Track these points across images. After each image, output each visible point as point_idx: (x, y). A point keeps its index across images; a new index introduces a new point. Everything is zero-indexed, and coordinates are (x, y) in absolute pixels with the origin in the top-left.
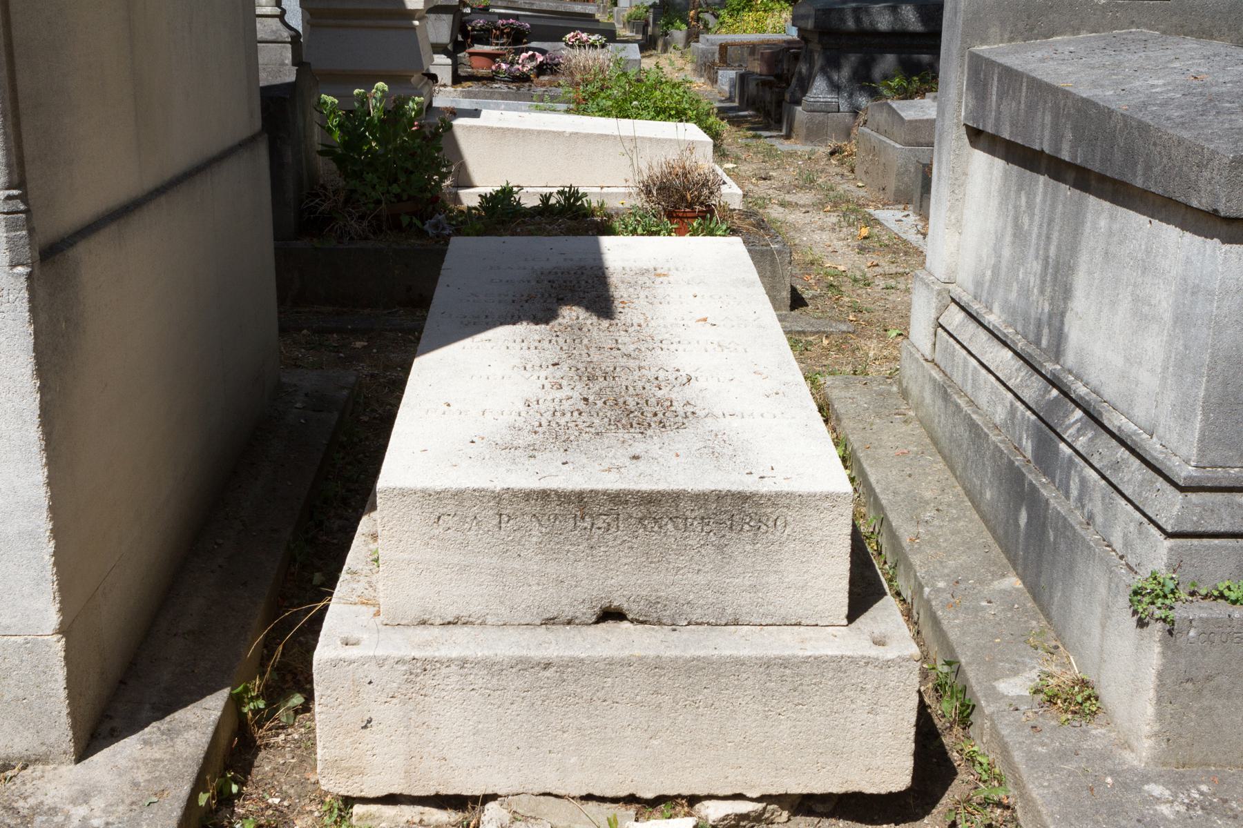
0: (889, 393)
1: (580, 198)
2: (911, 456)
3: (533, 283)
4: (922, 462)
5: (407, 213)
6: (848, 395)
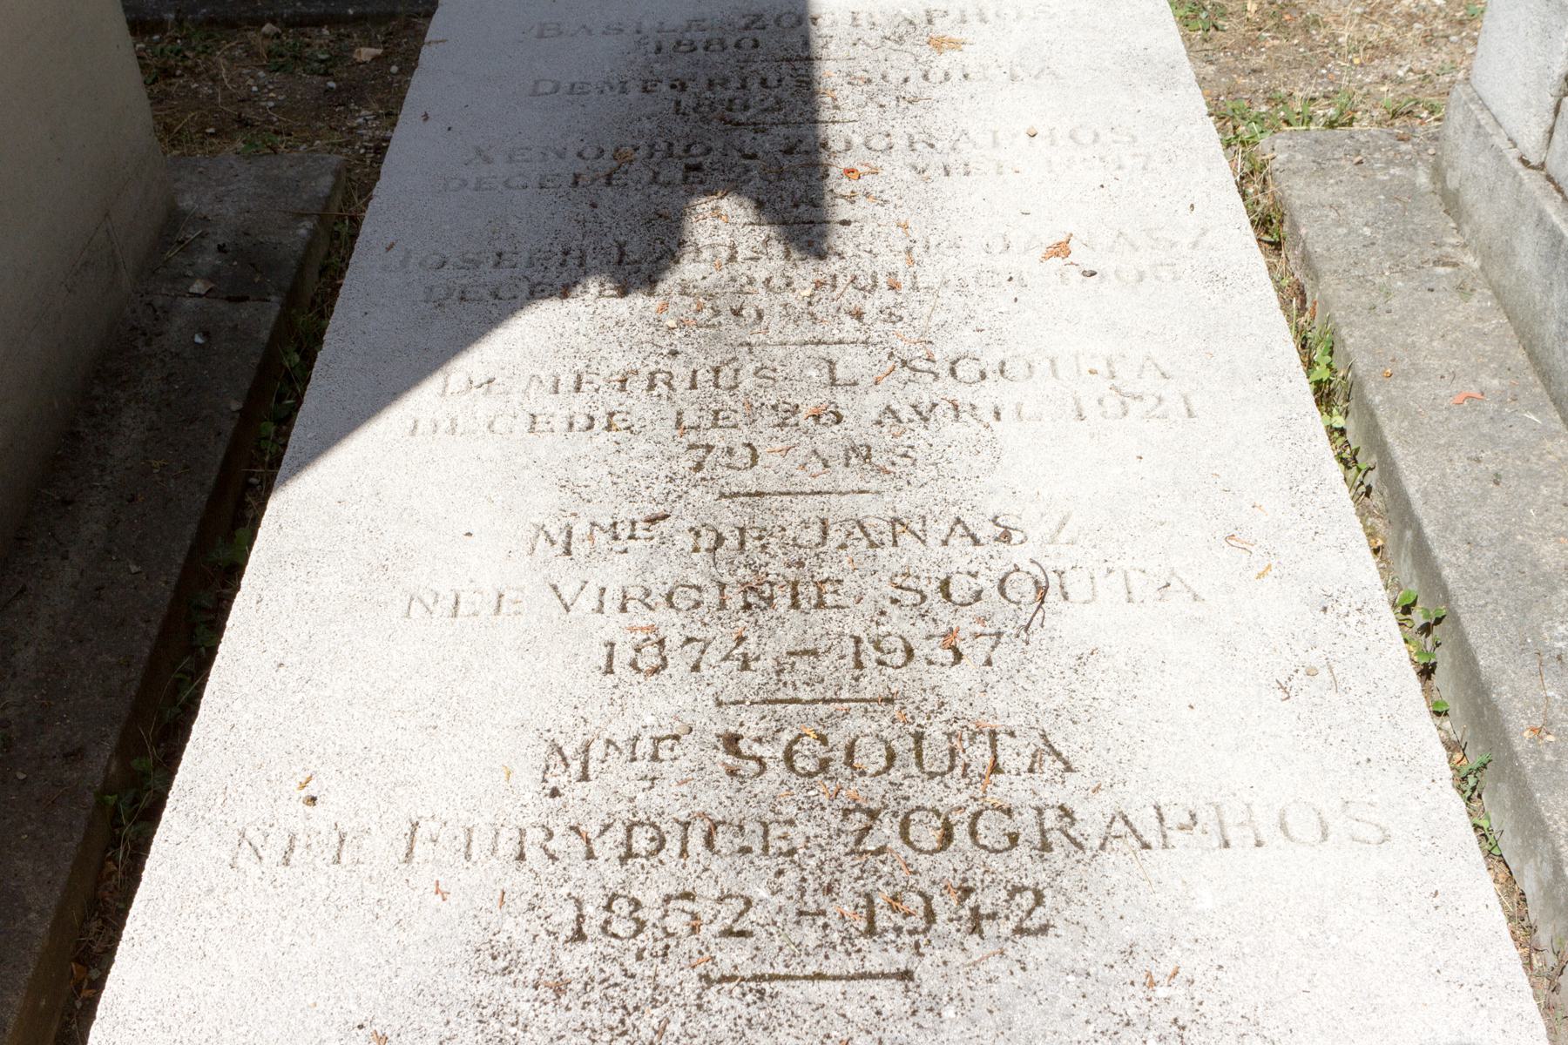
0: (1413, 189)
2: (1491, 406)
3: (634, 93)
4: (1519, 433)
6: (1326, 196)
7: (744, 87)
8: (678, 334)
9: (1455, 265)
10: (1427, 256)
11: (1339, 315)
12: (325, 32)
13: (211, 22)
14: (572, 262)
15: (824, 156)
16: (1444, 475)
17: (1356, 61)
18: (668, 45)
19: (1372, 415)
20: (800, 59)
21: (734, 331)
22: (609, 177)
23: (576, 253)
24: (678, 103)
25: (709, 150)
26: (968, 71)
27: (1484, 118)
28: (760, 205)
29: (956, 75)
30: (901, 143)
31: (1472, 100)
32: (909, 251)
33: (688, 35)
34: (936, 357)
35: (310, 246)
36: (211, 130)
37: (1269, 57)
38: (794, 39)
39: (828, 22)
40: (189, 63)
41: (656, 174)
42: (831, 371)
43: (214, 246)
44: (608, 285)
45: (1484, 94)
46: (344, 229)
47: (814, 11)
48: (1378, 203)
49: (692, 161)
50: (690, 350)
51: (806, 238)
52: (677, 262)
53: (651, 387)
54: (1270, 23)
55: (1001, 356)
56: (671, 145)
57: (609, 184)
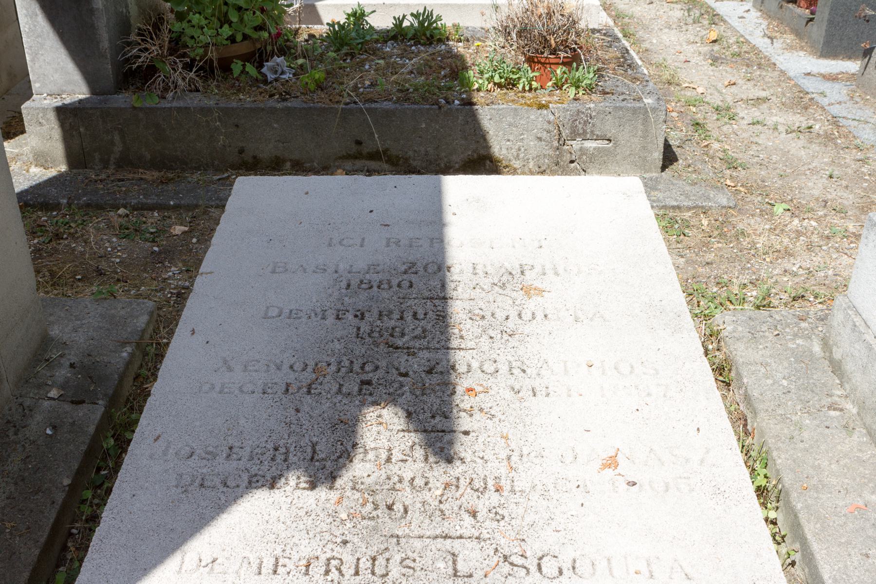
1: (435, 22)
3: (331, 320)
5: (238, 57)
7: (402, 318)
8: (349, 525)
9: (841, 410)
10: (823, 403)
11: (771, 441)
12: (156, 214)
13: (88, 205)
14: (280, 458)
15: (453, 376)
16: (846, 566)
17: (768, 260)
18: (354, 283)
19: (796, 516)
20: (439, 298)
21: (388, 525)
22: (309, 388)
23: (283, 450)
24: (359, 329)
25: (377, 368)
26: (548, 312)
27: (858, 320)
28: (409, 415)
29: (540, 316)
30: (504, 369)
31: (849, 307)
32: (509, 458)
33: (368, 276)
34: (528, 554)
35: (129, 363)
36: (79, 277)
37: (716, 255)
38: (435, 283)
39: (458, 271)
40: (72, 231)
41: (341, 385)
42: (454, 562)
43: (68, 363)
44: (303, 479)
45: (857, 305)
46: (152, 350)
47: (449, 262)
48: (790, 364)
49: (365, 377)
50: (356, 539)
51: (439, 445)
52: (351, 461)
53: (327, 572)
54: (716, 233)
55: (573, 555)
56: (352, 362)
57: (309, 392)
